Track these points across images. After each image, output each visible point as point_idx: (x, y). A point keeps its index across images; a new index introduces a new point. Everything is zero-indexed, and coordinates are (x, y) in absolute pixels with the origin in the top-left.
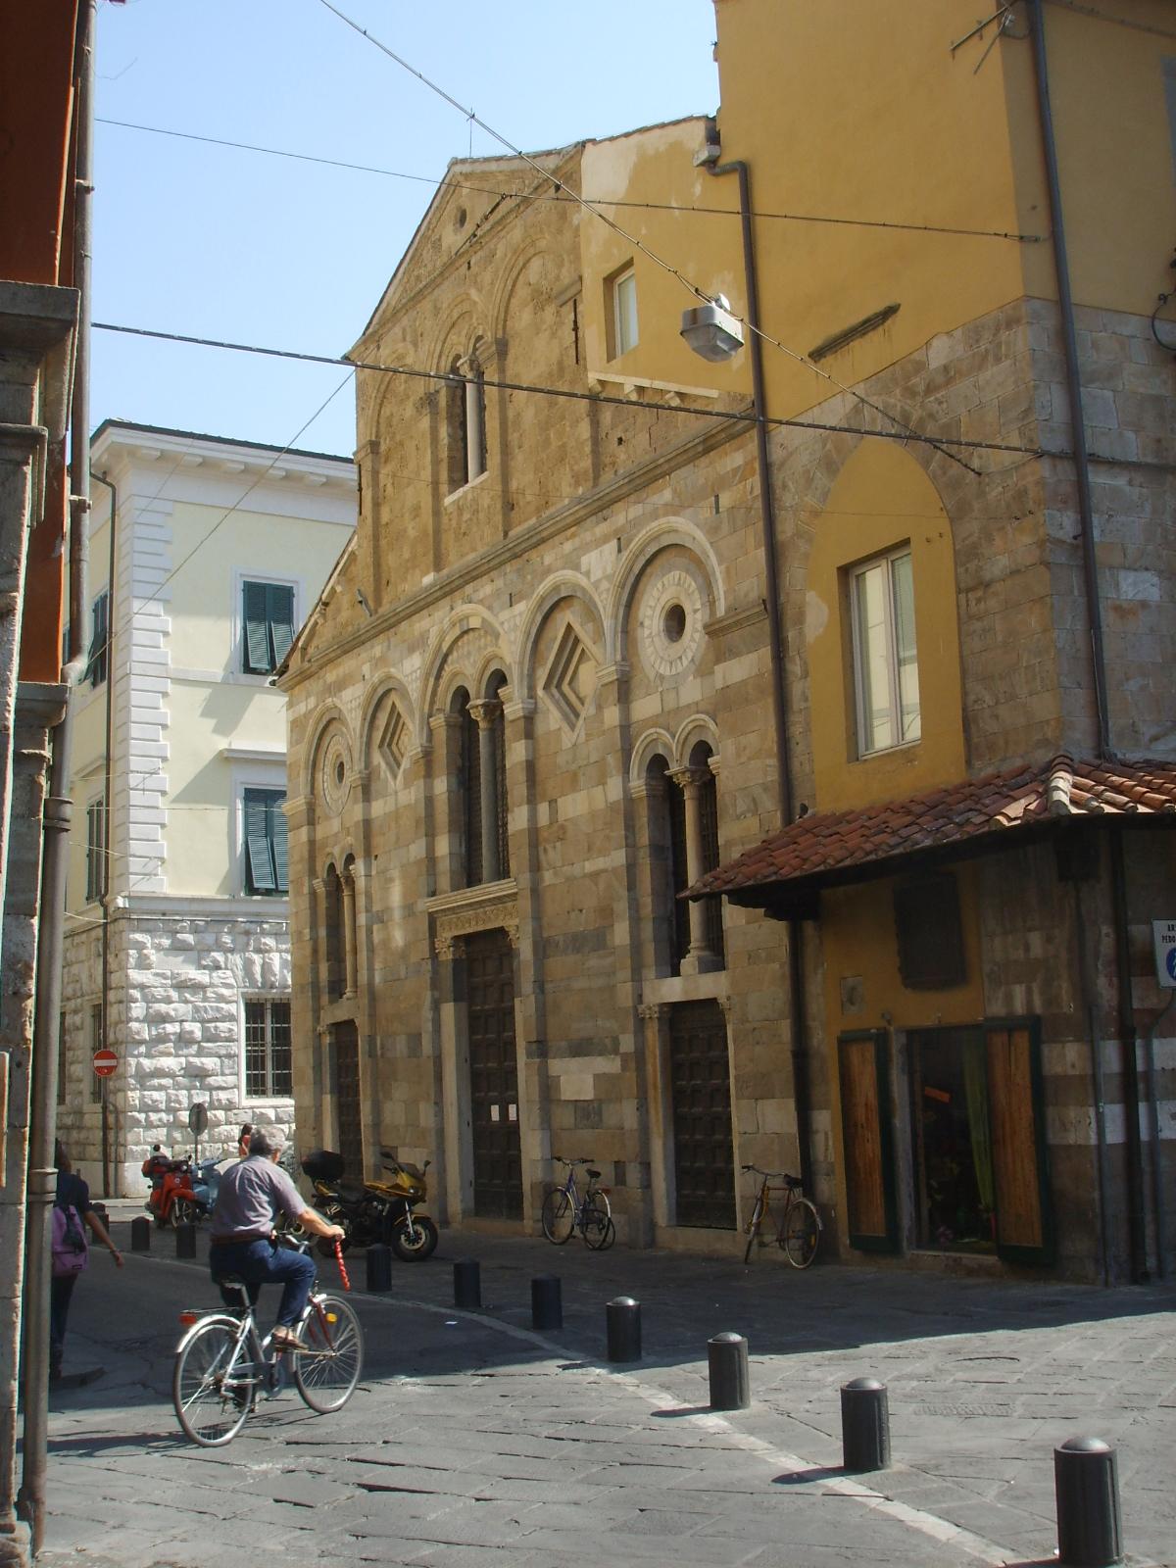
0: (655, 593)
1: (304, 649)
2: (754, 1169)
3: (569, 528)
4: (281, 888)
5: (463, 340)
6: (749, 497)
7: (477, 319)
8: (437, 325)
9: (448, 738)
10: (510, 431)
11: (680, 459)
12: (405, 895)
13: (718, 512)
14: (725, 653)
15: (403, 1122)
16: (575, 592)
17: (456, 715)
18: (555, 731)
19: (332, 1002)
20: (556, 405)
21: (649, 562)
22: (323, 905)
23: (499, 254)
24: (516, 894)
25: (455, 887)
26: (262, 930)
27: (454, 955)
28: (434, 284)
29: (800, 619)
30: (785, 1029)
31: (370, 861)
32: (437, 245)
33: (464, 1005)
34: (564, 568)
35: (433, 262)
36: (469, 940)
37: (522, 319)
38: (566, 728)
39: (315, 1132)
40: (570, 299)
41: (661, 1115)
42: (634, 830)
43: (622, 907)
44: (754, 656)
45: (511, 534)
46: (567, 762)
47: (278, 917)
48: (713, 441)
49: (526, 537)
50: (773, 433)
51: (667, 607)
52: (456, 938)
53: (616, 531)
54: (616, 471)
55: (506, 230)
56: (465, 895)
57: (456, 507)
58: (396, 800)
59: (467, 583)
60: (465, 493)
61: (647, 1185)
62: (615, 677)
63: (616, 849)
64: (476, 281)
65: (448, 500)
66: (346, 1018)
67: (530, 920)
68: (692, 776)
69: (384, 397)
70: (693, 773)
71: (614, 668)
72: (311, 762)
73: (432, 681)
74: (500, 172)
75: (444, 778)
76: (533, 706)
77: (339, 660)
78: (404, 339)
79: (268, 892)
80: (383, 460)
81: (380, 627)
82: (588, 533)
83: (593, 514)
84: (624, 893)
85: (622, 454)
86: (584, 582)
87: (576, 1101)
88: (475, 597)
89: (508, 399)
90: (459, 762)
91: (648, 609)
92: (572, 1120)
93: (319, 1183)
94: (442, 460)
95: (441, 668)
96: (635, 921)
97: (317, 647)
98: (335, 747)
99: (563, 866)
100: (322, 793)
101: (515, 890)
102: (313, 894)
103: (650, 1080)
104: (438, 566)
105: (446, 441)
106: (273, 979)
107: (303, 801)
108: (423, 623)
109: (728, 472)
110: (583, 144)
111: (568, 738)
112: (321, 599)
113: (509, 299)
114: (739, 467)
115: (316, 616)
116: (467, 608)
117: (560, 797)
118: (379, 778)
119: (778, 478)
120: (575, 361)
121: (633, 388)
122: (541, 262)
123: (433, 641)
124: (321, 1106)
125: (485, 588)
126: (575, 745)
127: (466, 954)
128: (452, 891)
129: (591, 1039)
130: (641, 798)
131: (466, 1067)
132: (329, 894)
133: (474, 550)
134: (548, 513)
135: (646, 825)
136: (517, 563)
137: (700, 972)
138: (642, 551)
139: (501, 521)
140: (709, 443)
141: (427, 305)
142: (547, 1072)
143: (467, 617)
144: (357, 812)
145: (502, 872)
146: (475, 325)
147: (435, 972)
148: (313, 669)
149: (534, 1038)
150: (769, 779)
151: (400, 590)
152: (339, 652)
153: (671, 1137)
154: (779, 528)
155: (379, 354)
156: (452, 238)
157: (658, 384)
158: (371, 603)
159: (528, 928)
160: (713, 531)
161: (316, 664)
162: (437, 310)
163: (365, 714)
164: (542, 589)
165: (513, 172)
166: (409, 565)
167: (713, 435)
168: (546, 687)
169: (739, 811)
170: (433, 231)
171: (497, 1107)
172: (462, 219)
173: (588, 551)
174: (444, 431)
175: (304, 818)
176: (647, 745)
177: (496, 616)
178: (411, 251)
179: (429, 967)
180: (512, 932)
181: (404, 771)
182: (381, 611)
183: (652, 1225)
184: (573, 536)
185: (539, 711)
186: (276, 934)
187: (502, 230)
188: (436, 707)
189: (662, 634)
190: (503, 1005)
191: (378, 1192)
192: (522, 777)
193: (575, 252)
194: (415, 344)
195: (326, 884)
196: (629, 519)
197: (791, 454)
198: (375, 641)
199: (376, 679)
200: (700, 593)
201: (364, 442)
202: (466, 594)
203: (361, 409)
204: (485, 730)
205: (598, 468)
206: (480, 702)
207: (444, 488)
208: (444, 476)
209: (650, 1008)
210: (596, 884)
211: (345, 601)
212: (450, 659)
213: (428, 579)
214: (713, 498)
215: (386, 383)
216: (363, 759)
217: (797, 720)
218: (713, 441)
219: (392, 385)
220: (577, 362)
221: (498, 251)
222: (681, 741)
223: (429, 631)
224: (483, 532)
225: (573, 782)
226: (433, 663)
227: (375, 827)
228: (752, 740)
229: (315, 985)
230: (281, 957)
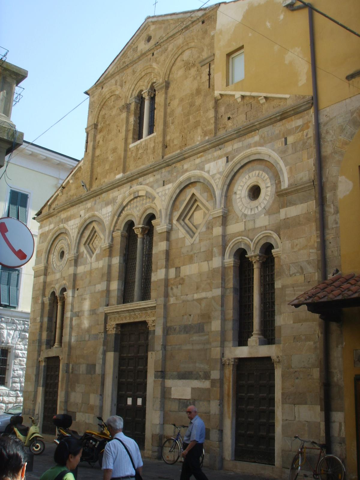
0: (244, 180)
1: (50, 206)
2: (298, 438)
3: (200, 153)
4: (11, 305)
5: (146, 84)
6: (305, 138)
7: (154, 75)
8: (134, 78)
9: (121, 241)
10: (168, 117)
11: (267, 123)
12: (91, 305)
13: (286, 144)
15: (80, 402)
16: (200, 180)
17: (125, 232)
18: (181, 238)
19: (47, 348)
20: (194, 105)
21: (242, 167)
22: (47, 308)
23: (169, 49)
24: (155, 307)
25: (118, 303)
26: (2, 320)
27: (116, 331)
28: (134, 62)
29: (335, 187)
30: (316, 373)
31: (75, 290)
32: (135, 50)
33: (117, 354)
34: (195, 170)
35: (132, 56)
36: (122, 326)
37: (178, 73)
38: (188, 236)
39: (33, 402)
40: (207, 63)
41: (231, 408)
42: (225, 281)
43: (217, 314)
44: (305, 205)
45: (165, 157)
47: (8, 316)
48: (286, 115)
49: (177, 156)
50: (321, 111)
51: (250, 186)
52: (117, 325)
53: (225, 154)
54: (226, 130)
55: (174, 40)
56: (126, 306)
57: (135, 148)
58: (91, 266)
59: (141, 177)
60: (141, 143)
61: (221, 440)
62: (221, 214)
63: (214, 289)
64: (156, 60)
65: (132, 146)
66: (54, 355)
67: (162, 318)
68: (259, 258)
69: (102, 108)
70: (260, 256)
71: (221, 210)
72: (48, 251)
73: (116, 217)
74: (172, 19)
75: (118, 258)
76: (170, 228)
77: (68, 209)
78: (116, 84)
79: (5, 306)
80: (99, 131)
81: (92, 196)
82: (210, 155)
83: (214, 147)
84: (220, 308)
85: (230, 124)
86: (206, 175)
87: (180, 399)
88: (144, 183)
89: (168, 105)
90: (125, 252)
91: (240, 187)
92: (177, 407)
93: (60, 429)
94: (130, 130)
95: (121, 212)
96: (224, 320)
97: (58, 204)
98: (61, 244)
99: (182, 295)
100: (52, 263)
101: (156, 305)
102: (43, 303)
103: (226, 392)
104: (124, 171)
105: (133, 123)
106: (3, 340)
107: (43, 265)
108: (114, 194)
109: (293, 128)
110: (220, 4)
111: (189, 241)
112: (62, 185)
113: (172, 67)
114: (299, 126)
115: (58, 192)
116: (139, 187)
117: (182, 266)
118: (83, 257)
119: (323, 130)
120: (208, 87)
121: (240, 96)
122: (190, 52)
123: (119, 200)
124: (37, 391)
125: (150, 179)
127: (121, 332)
128: (117, 304)
129: (192, 372)
130: (230, 267)
131: (116, 380)
132: (50, 304)
133: (143, 164)
134: (186, 148)
135: (232, 279)
136: (168, 169)
137: (259, 345)
138: (239, 162)
139: (161, 152)
140: (283, 116)
141: (129, 71)
142: (164, 385)
143: (138, 191)
144: (71, 270)
145: (145, 295)
146: (153, 78)
147: (105, 338)
148: (55, 213)
149: (160, 369)
150: (311, 258)
151: (102, 181)
152: (69, 205)
153: (234, 419)
154: (323, 150)
155: (102, 91)
156: (143, 46)
157: (254, 94)
158: (88, 186)
159: (161, 321)
160: (283, 153)
161: (57, 210)
162: (134, 72)
163: (79, 231)
164: (181, 179)
165: (178, 19)
166: (108, 171)
167: (287, 112)
168: (178, 220)
169: (291, 273)
170: (134, 44)
171: (141, 399)
172: (149, 39)
174: (132, 119)
175: (43, 273)
176: (236, 244)
177: (155, 190)
178: (123, 52)
179: (103, 336)
180: (150, 323)
182: (92, 190)
183: (222, 459)
184: (201, 157)
185: (173, 230)
186: (7, 323)
187: (172, 40)
188: (117, 228)
189: (247, 197)
190: (139, 355)
191: (93, 436)
192: (163, 257)
193: (211, 46)
194: (121, 86)
195: (50, 300)
196: (234, 149)
197: (332, 119)
198: (88, 201)
199: (87, 216)
200: (270, 179)
201: (91, 124)
202: (139, 181)
203: (91, 111)
204: (141, 238)
205: (216, 129)
206: (141, 226)
207: (130, 140)
208: (131, 135)
209: (229, 360)
210: (200, 304)
211: (73, 187)
212: (126, 209)
213: (119, 176)
214: (284, 139)
215: (104, 102)
216: (76, 249)
217: (330, 232)
218: (286, 115)
219: (107, 103)
220: (209, 88)
221: (169, 48)
222: (256, 242)
223: (117, 196)
224: (149, 157)
225: (191, 259)
226: (117, 210)
227: (78, 277)
228: (302, 241)
229: (40, 341)
230: (7, 332)
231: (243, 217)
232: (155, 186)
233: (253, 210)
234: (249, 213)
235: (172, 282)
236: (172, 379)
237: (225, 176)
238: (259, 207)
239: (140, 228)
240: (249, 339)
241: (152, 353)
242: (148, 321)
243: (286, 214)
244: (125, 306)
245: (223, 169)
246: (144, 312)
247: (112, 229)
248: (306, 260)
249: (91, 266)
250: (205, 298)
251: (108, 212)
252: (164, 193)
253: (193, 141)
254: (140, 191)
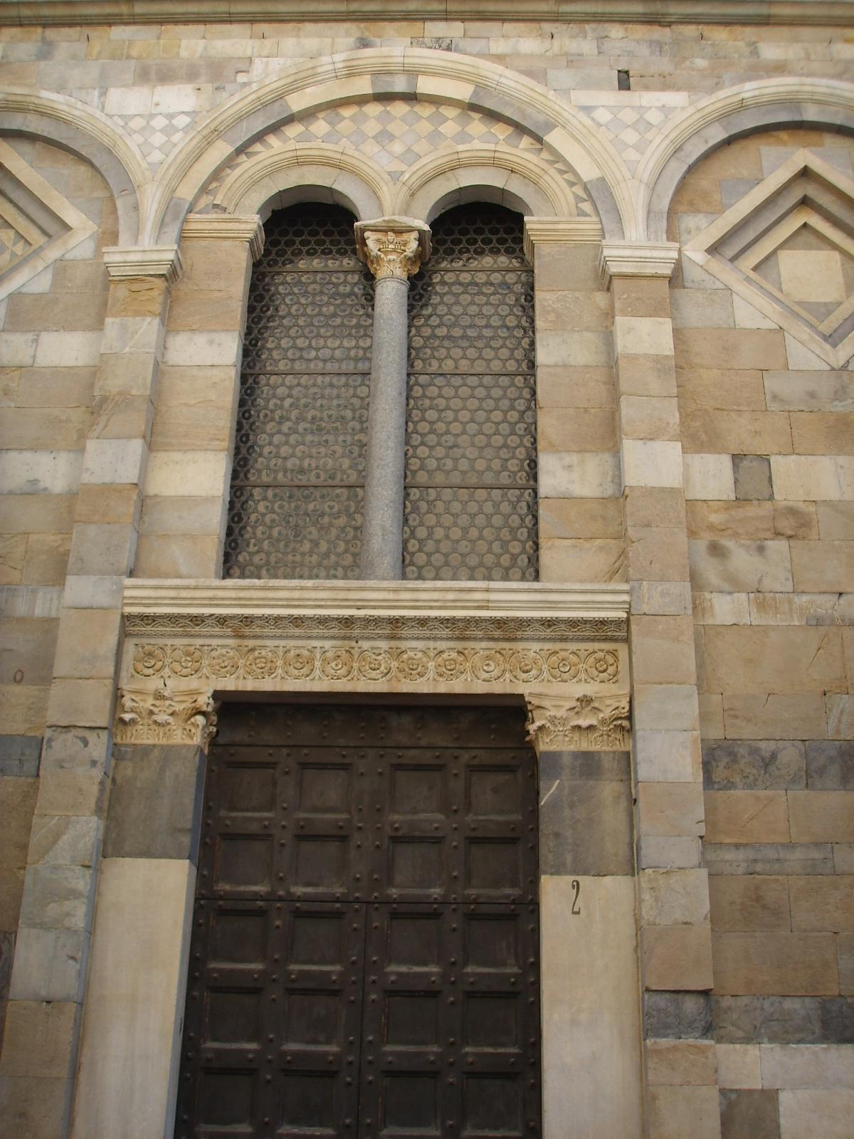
73: (222, 150)
95: (259, 137)
164: (751, 89)
212: (293, 130)
232: (562, 77)
235: (715, 518)
236: (772, 1039)
239: (415, 235)
241: (577, 886)
242: (539, 695)
244: (342, 595)
246: (484, 644)
247: (187, 192)
252: (628, 116)
254: (424, 73)
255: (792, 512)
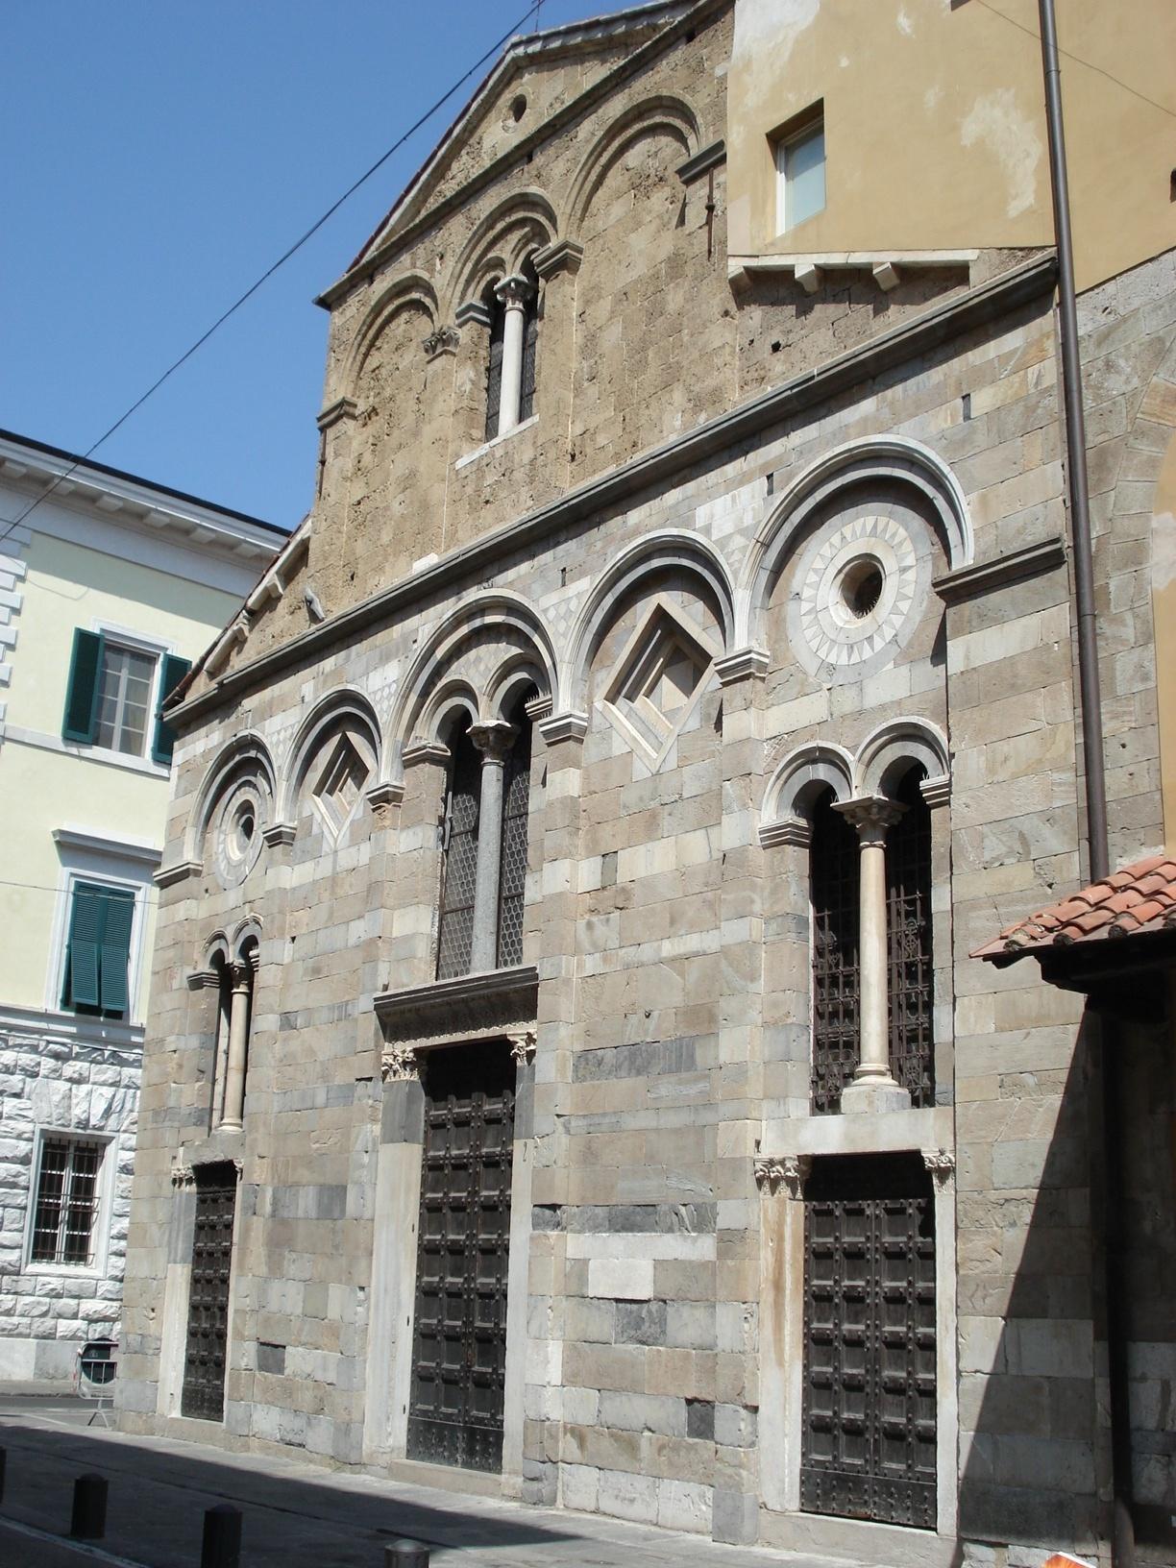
0: (826, 551)
14: (969, 622)
15: (299, 1311)
20: (662, 314)
46: (641, 799)
53: (763, 467)
58: (335, 862)
126: (658, 773)
169: (987, 856)
173: (711, 498)
181: (352, 822)
200: (913, 541)
231: (824, 676)
233: (855, 649)
234: (844, 660)
237: (761, 540)
238: (877, 639)
240: (846, 1091)
243: (967, 657)
245: (754, 519)
248: (1040, 808)
249: (335, 862)
250: (697, 954)
251: (389, 681)
253: (656, 430)
255: (623, 889)
